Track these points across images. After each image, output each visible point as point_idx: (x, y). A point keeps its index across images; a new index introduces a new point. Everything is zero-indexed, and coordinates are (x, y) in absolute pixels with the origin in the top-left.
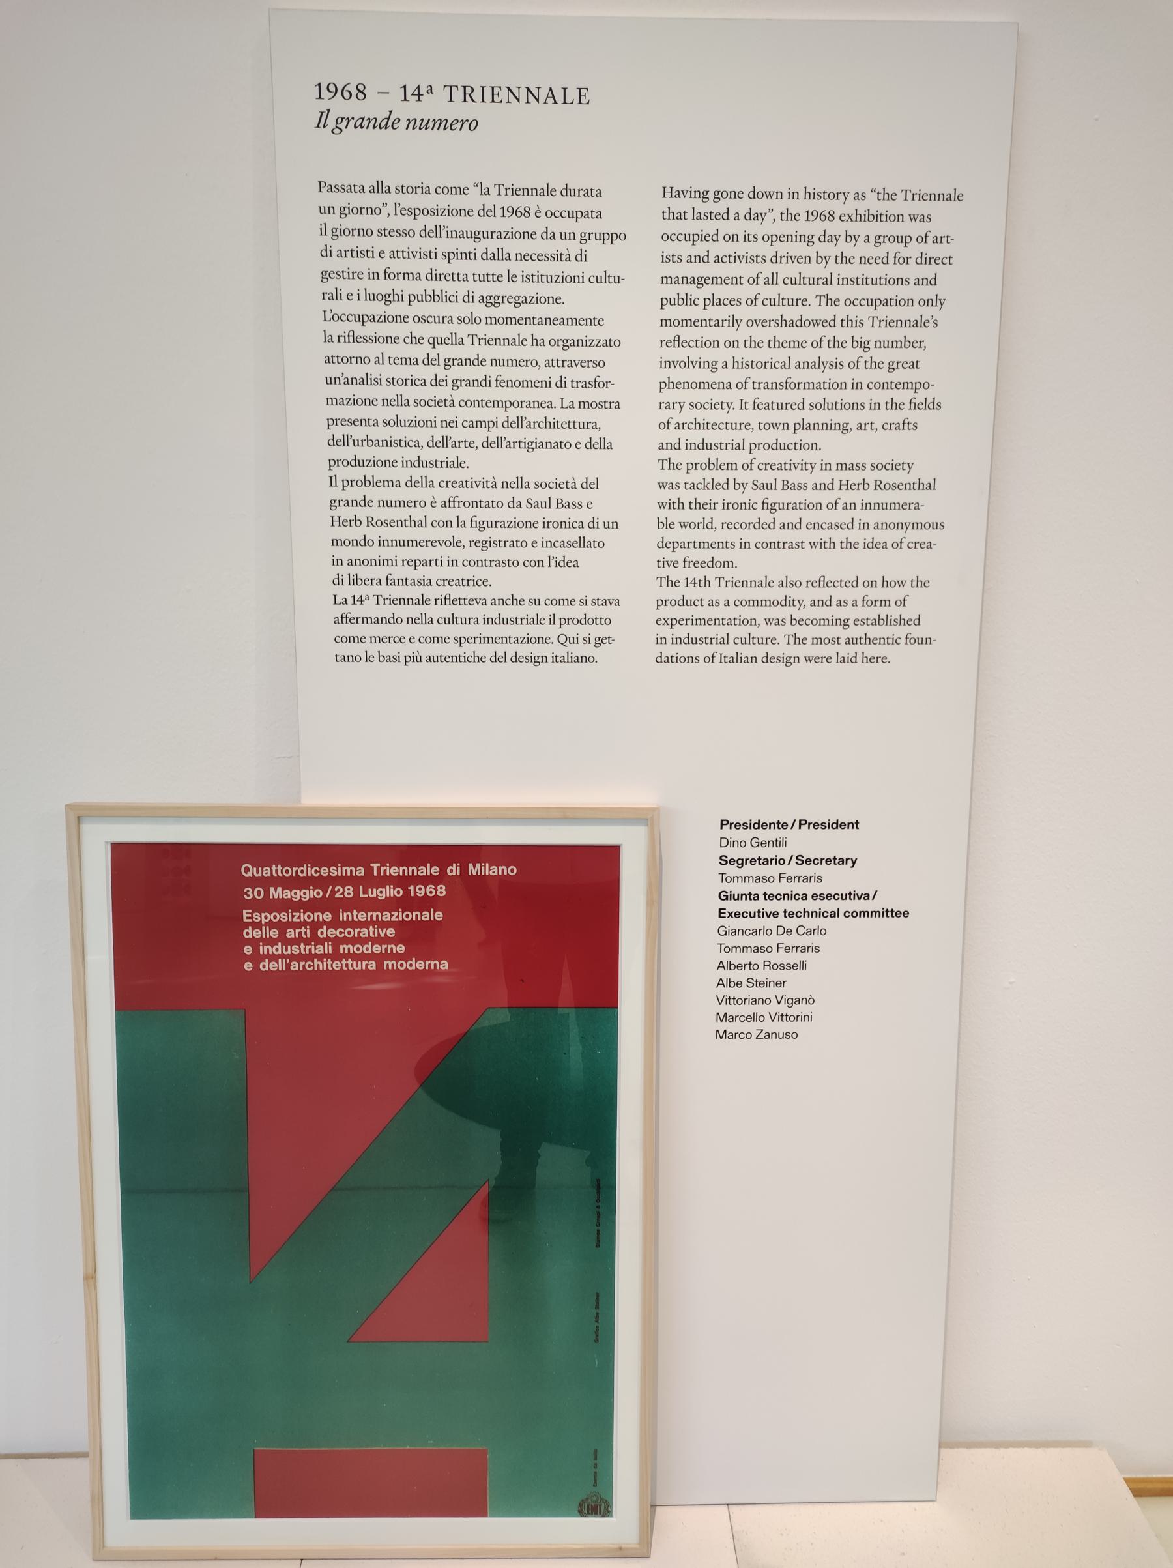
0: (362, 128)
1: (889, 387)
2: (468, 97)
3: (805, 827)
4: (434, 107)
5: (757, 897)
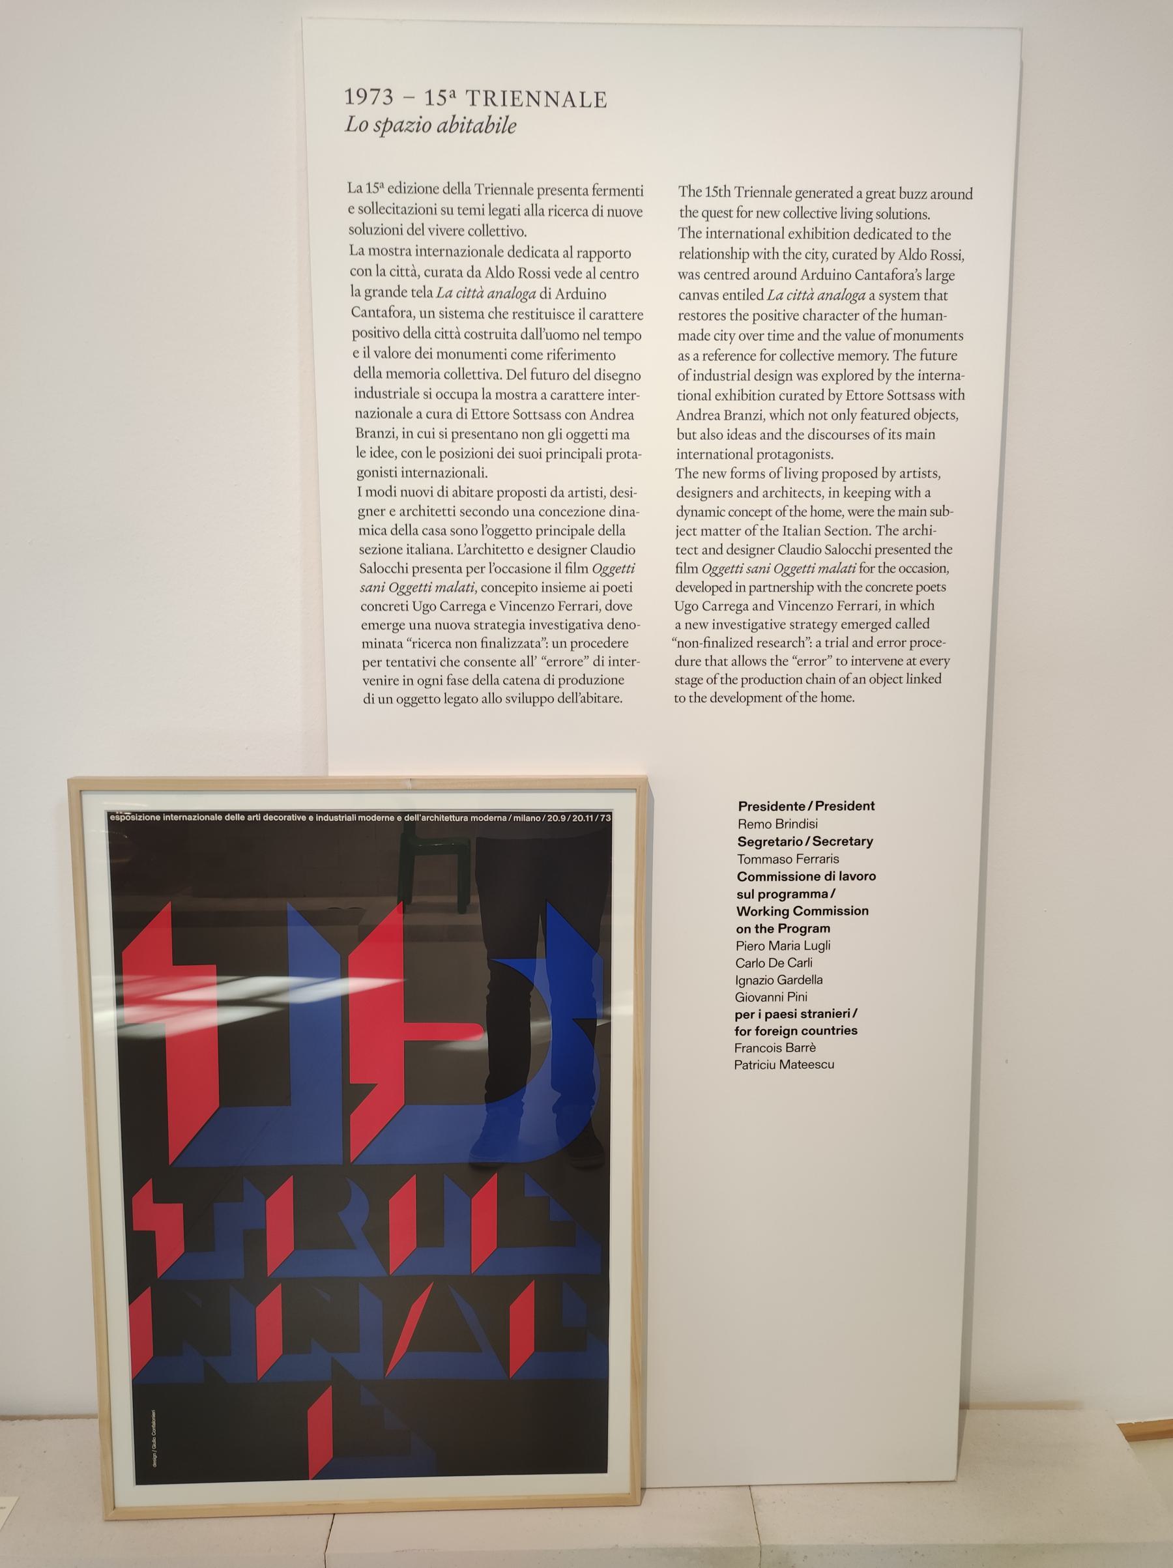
3: (821, 809)
4: (460, 108)
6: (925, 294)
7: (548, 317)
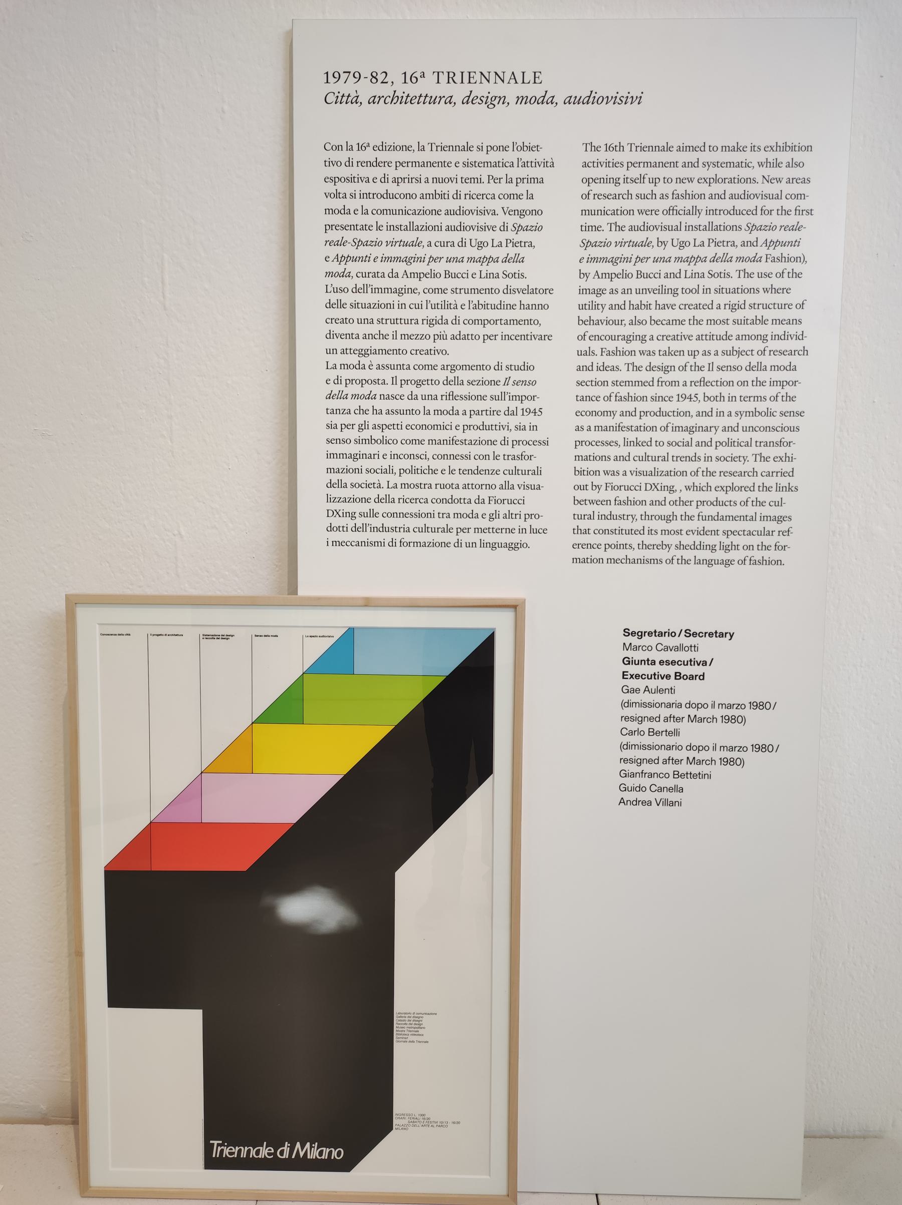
0: (374, 103)
2: (451, 80)
4: (427, 86)
5: (654, 663)
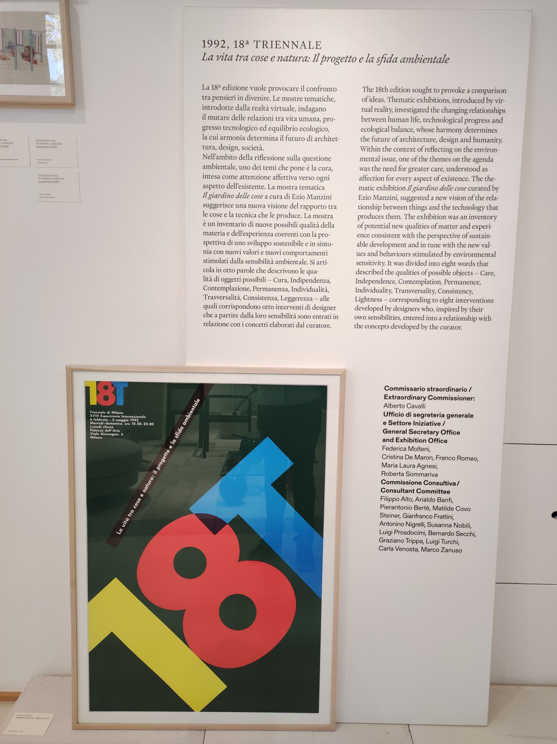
1: (325, 245)
2: (265, 46)
6: (361, 138)
7: (207, 148)
